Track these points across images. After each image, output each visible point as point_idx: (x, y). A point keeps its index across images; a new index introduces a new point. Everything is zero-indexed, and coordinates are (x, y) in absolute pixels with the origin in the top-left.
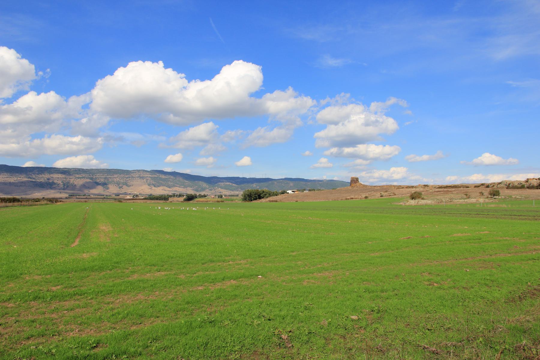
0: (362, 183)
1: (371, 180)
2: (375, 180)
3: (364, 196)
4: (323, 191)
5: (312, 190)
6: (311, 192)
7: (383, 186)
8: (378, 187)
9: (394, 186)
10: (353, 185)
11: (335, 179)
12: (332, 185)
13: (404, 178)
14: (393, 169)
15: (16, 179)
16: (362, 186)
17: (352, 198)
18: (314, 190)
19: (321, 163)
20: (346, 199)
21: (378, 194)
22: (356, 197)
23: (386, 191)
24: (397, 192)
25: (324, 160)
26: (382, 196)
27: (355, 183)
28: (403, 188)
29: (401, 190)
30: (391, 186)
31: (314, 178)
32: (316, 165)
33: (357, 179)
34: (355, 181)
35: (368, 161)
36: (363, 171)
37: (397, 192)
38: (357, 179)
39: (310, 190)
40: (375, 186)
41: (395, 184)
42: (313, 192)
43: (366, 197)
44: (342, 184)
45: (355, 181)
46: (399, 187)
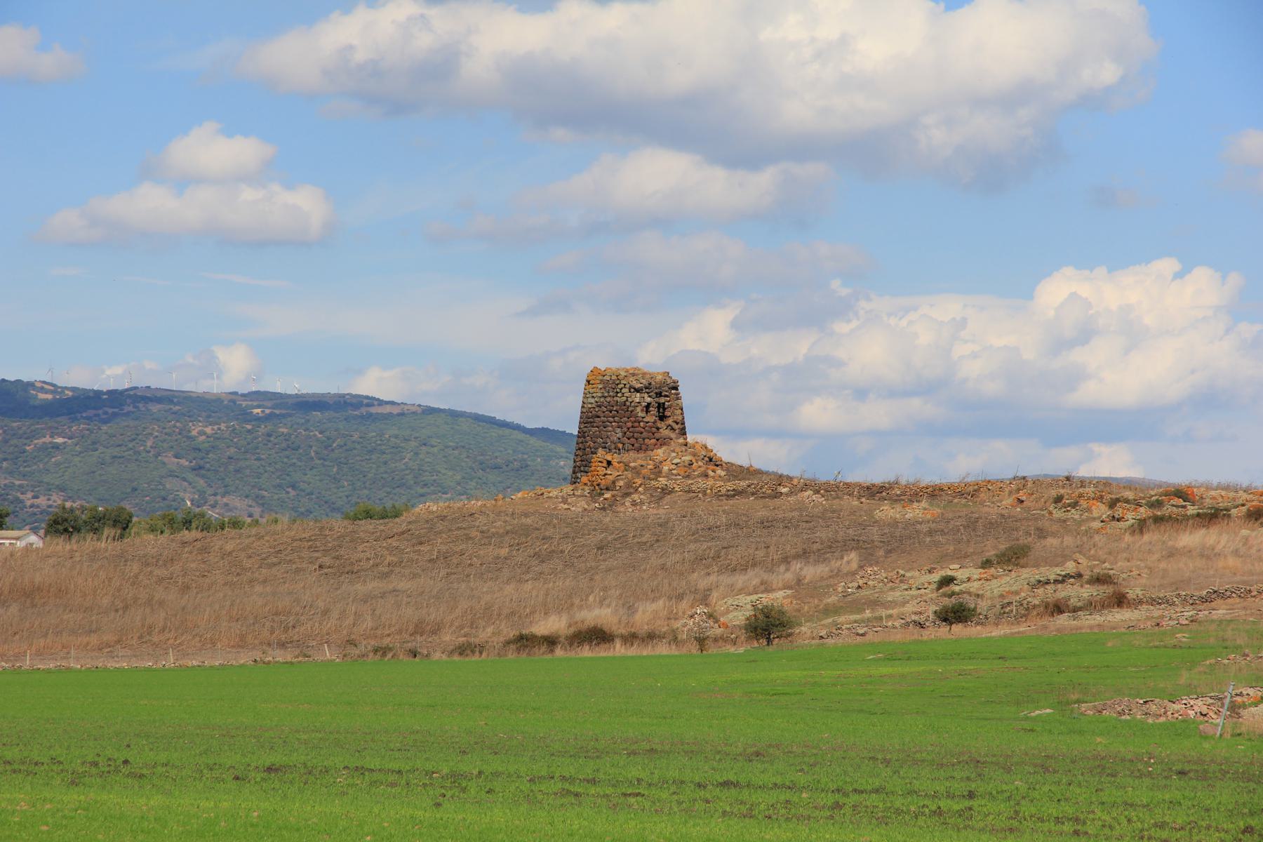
0: (727, 451)
1: (818, 413)
2: (877, 414)
3: (737, 610)
4: (228, 542)
5: (96, 524)
6: (87, 544)
7: (969, 492)
8: (914, 493)
9: (1112, 495)
10: (616, 465)
11: (373, 383)
12: (332, 467)
13: (1210, 400)
14: (1059, 291)
15: (1110, 618)
16: (717, 481)
17: (598, 636)
18: (122, 523)
19: (184, 182)
20: (525, 642)
21: (915, 592)
22: (647, 614)
23: (1014, 557)
24: (1140, 560)
25: (212, 150)
26: (956, 615)
27: (640, 439)
28: (1213, 516)
29: (1190, 539)
30: (1068, 494)
31: (111, 375)
32: (150, 203)
33: (662, 399)
34: (632, 414)
35: (760, 185)
36: (697, 290)
37: (1140, 560)
38: (662, 399)
39: (61, 526)
40: (874, 492)
41: (1112, 463)
42: (106, 543)
43: (767, 627)
44: (479, 446)
45: (632, 414)
46: (1171, 508)
